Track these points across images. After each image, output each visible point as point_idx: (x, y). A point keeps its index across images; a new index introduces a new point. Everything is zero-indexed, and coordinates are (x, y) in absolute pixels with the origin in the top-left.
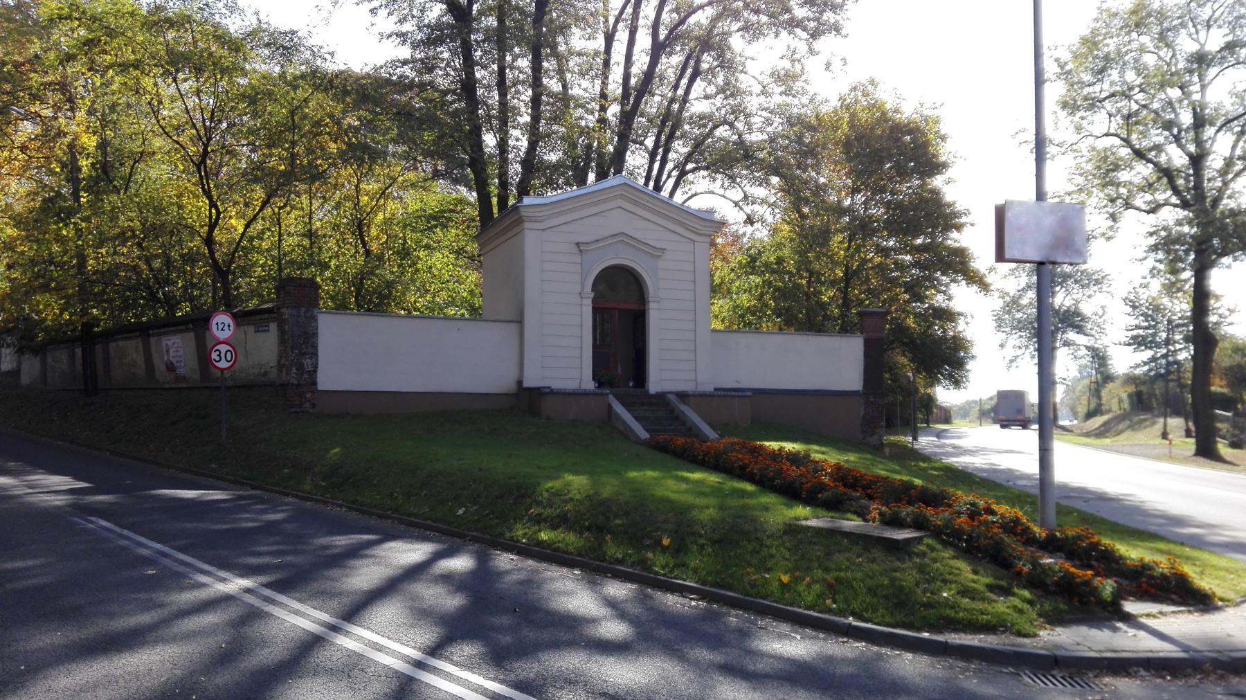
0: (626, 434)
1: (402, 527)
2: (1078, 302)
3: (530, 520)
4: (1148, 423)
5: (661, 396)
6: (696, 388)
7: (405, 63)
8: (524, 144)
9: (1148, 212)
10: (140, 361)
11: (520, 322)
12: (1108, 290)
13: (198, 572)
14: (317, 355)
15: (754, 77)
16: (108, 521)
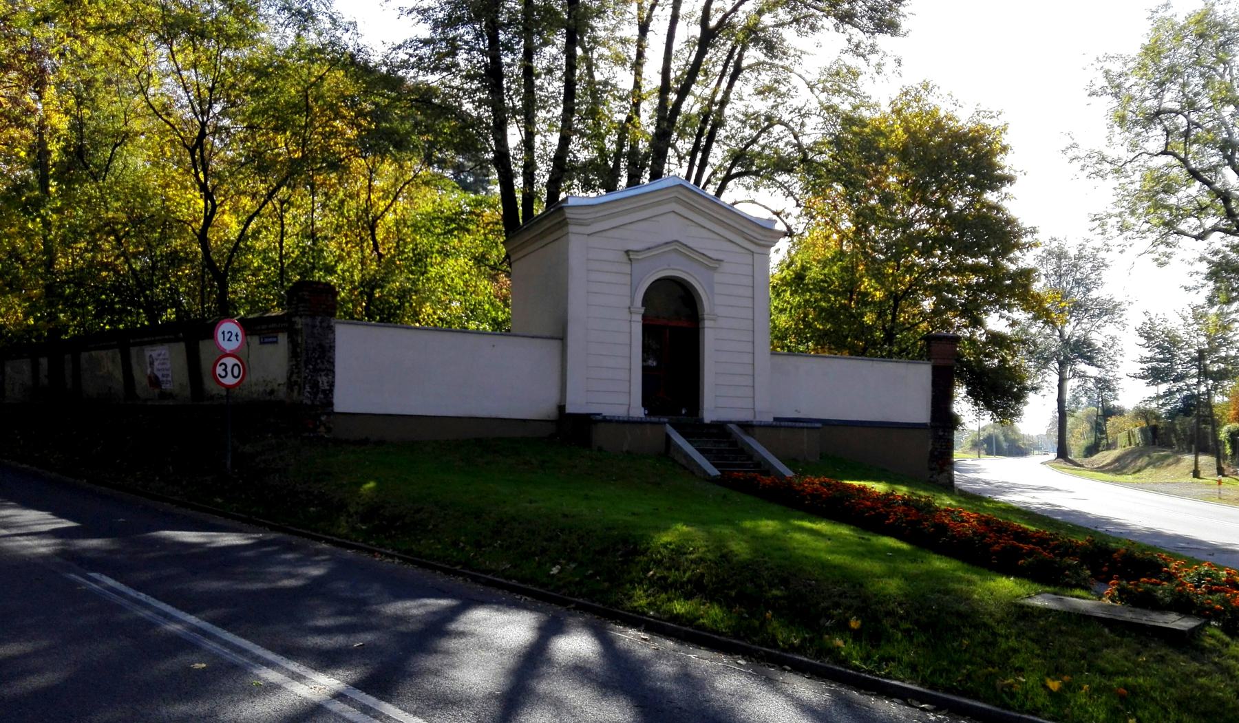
0: (690, 468)
1: (480, 588)
2: (1087, 332)
3: (652, 584)
4: (1171, 460)
5: (720, 428)
6: (755, 417)
7: (426, 42)
8: (555, 139)
9: (1198, 238)
10: (118, 374)
11: (562, 338)
12: (1119, 320)
13: (263, 664)
14: (334, 372)
15: (800, 76)
16: (116, 580)
